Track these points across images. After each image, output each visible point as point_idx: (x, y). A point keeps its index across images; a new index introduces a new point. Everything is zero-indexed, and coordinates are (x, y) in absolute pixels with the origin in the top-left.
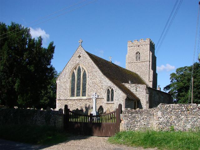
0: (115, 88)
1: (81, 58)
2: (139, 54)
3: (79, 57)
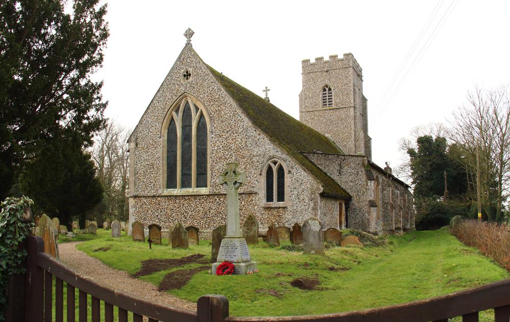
1: (191, 79)
2: (330, 89)
3: (185, 76)
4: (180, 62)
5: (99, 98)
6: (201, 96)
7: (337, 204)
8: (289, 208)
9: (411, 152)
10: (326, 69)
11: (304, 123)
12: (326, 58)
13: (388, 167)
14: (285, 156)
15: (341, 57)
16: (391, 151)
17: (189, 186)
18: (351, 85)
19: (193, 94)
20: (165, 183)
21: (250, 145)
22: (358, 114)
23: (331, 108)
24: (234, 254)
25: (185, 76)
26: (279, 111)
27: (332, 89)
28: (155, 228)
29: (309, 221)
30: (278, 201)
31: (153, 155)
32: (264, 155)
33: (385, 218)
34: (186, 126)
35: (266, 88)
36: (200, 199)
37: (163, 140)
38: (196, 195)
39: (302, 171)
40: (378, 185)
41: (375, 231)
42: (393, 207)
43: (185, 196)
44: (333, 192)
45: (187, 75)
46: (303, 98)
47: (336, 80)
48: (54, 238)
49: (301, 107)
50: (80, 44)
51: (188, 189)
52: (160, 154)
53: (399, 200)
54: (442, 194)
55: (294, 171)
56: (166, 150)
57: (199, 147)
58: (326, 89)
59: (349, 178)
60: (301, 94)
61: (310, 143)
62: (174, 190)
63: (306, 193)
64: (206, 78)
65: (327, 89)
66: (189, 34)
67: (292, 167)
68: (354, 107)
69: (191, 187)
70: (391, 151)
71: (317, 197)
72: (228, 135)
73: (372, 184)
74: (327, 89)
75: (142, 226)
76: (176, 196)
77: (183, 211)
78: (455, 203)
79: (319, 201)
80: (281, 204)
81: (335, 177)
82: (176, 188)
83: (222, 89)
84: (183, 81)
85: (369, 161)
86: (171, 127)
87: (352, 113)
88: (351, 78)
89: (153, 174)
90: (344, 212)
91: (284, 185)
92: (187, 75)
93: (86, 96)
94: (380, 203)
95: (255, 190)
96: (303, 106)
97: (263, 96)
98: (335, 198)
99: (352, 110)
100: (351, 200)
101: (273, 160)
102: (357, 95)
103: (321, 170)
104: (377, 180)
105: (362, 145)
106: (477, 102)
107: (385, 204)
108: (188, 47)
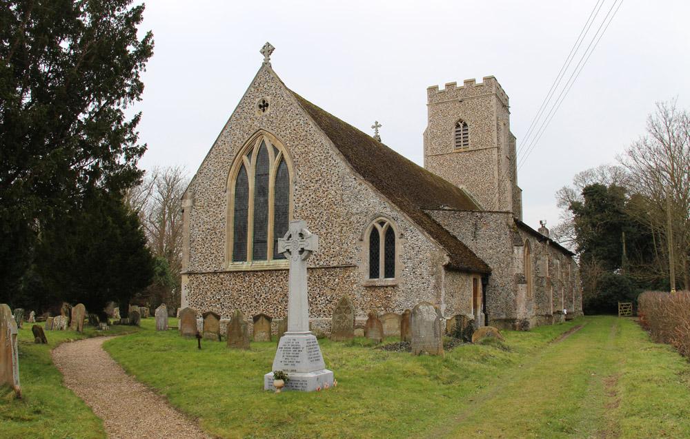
0: (401, 222)
1: (268, 111)
2: (465, 125)
3: (260, 106)
4: (255, 88)
5: (133, 139)
6: (282, 133)
7: (470, 280)
8: (401, 288)
9: (575, 207)
10: (460, 99)
11: (430, 170)
12: (460, 84)
13: (543, 227)
14: (396, 213)
15: (479, 81)
16: (546, 210)
17: (264, 257)
18: (494, 118)
19: (271, 131)
20: (231, 254)
21: (348, 199)
22: (503, 157)
23: (467, 149)
24: (298, 359)
25: (260, 106)
26: (396, 154)
27: (468, 125)
28: (212, 316)
29: (421, 307)
30: (386, 277)
31: (215, 214)
32: (367, 213)
33: (540, 297)
34: (261, 177)
35: (377, 123)
36: (277, 276)
37: (230, 196)
38: (273, 270)
39: (420, 234)
40: (529, 252)
41: (524, 317)
42: (550, 284)
43: (257, 271)
44: (465, 264)
45: (264, 106)
46: (429, 136)
47: (471, 112)
48: (11, 339)
49: (426, 149)
50: (114, 60)
51: (262, 262)
52: (225, 214)
53: (559, 273)
54: (619, 264)
55: (408, 235)
56: (232, 208)
57: (278, 204)
58: (461, 125)
59: (488, 245)
60: (426, 131)
61: (429, 196)
62: (243, 264)
63: (424, 265)
64: (289, 108)
65: (461, 125)
66: (268, 50)
67: (406, 229)
68: (498, 148)
69: (266, 259)
70: (546, 210)
71: (440, 271)
72: (317, 186)
73: (519, 252)
74: (461, 125)
75: (194, 314)
76: (245, 272)
77: (254, 293)
78: (638, 276)
79: (443, 276)
80: (390, 281)
81: (468, 242)
82: (246, 261)
83: (311, 123)
84: (258, 113)
85: (516, 221)
86: (241, 176)
87: (495, 157)
88: (494, 109)
89: (214, 241)
90: (480, 291)
91: (394, 254)
92: (264, 106)
93: (112, 134)
94: (531, 278)
95: (354, 262)
96: (429, 148)
97: (371, 133)
98: (468, 272)
99: (495, 151)
100: (490, 274)
101: (378, 219)
102: (502, 133)
103: (447, 232)
104: (528, 244)
105: (509, 199)
106: (666, 137)
107: (539, 280)
108: (266, 68)
